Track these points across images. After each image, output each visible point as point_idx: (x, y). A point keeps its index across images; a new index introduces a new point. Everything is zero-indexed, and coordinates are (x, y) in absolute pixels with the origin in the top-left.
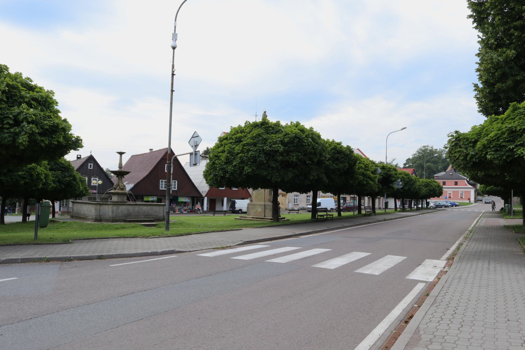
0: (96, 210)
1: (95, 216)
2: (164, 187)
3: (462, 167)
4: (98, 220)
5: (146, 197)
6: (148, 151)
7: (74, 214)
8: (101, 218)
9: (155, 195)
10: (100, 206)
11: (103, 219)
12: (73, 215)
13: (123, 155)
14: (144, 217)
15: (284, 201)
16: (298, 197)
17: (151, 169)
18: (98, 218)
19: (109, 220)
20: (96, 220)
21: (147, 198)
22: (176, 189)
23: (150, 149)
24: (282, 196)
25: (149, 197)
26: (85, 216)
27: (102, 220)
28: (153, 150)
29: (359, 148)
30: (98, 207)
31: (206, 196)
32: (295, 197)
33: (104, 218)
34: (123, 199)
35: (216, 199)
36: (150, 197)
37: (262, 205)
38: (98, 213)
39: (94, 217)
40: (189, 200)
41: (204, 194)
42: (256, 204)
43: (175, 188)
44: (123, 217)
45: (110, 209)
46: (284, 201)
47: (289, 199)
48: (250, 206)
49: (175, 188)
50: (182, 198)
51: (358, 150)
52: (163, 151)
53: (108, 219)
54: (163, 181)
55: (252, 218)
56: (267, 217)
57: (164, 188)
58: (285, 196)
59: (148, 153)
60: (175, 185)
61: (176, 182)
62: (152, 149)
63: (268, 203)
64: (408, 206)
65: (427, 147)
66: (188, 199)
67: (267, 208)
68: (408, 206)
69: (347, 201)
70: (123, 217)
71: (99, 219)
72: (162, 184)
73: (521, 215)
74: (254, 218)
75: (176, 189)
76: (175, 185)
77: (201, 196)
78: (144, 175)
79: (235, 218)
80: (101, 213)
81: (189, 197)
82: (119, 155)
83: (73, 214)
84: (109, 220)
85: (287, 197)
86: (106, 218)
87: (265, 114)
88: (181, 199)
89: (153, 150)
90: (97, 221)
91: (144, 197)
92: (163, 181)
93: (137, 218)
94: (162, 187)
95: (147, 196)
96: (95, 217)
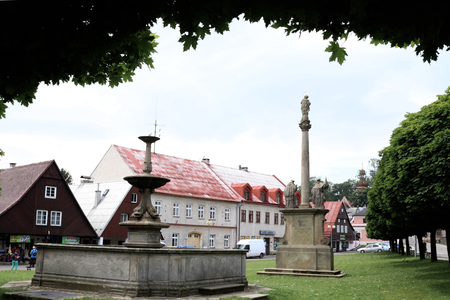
0: (140, 268)
1: (137, 283)
2: (42, 221)
3: (423, 200)
4: (145, 292)
5: (13, 237)
6: (9, 167)
7: (43, 275)
8: (151, 287)
9: (28, 233)
10: (148, 258)
11: (157, 290)
12: (43, 279)
13: (153, 144)
14: (223, 280)
15: (198, 243)
16: (214, 238)
17: (23, 192)
18: (145, 288)
19: (172, 292)
20: (140, 292)
21: (15, 238)
22: (60, 225)
23: (11, 164)
24: (195, 237)
25: (18, 237)
26: (95, 282)
27: (153, 292)
28: (16, 165)
29: (274, 175)
30: (144, 259)
31: (102, 236)
32: (225, 238)
33: (159, 288)
34: (155, 241)
35: (110, 240)
36: (20, 237)
37: (312, 250)
38: (145, 275)
39: (136, 286)
40: (77, 241)
41: (99, 233)
42: (299, 249)
43: (59, 224)
44: (196, 282)
45: (175, 265)
46: (198, 243)
47: (203, 241)
48: (283, 252)
49: (58, 223)
50: (68, 239)
51: (273, 177)
52: (40, 166)
53: (169, 290)
54: (41, 212)
55: (294, 271)
56: (322, 269)
57: (42, 223)
58: (198, 237)
59: (8, 170)
60: (58, 218)
61: (60, 213)
62: (15, 164)
63: (320, 246)
64: (336, 249)
65: (314, 179)
66: (76, 240)
67: (320, 254)
68: (336, 249)
69: (270, 242)
70: (196, 282)
71: (146, 290)
72: (39, 217)
73: (440, 257)
74: (299, 272)
75: (60, 225)
76: (58, 218)
77: (95, 236)
78: (13, 203)
79: (258, 273)
80: (150, 275)
81: (78, 237)
82: (145, 144)
83: (41, 277)
84: (172, 292)
85: (201, 238)
86: (163, 288)
87: (306, 100)
88: (66, 240)
89: (16, 165)
90: (143, 294)
91: (11, 236)
92: (41, 212)
93: (225, 281)
94: (39, 222)
95: (16, 234)
96: (139, 285)
